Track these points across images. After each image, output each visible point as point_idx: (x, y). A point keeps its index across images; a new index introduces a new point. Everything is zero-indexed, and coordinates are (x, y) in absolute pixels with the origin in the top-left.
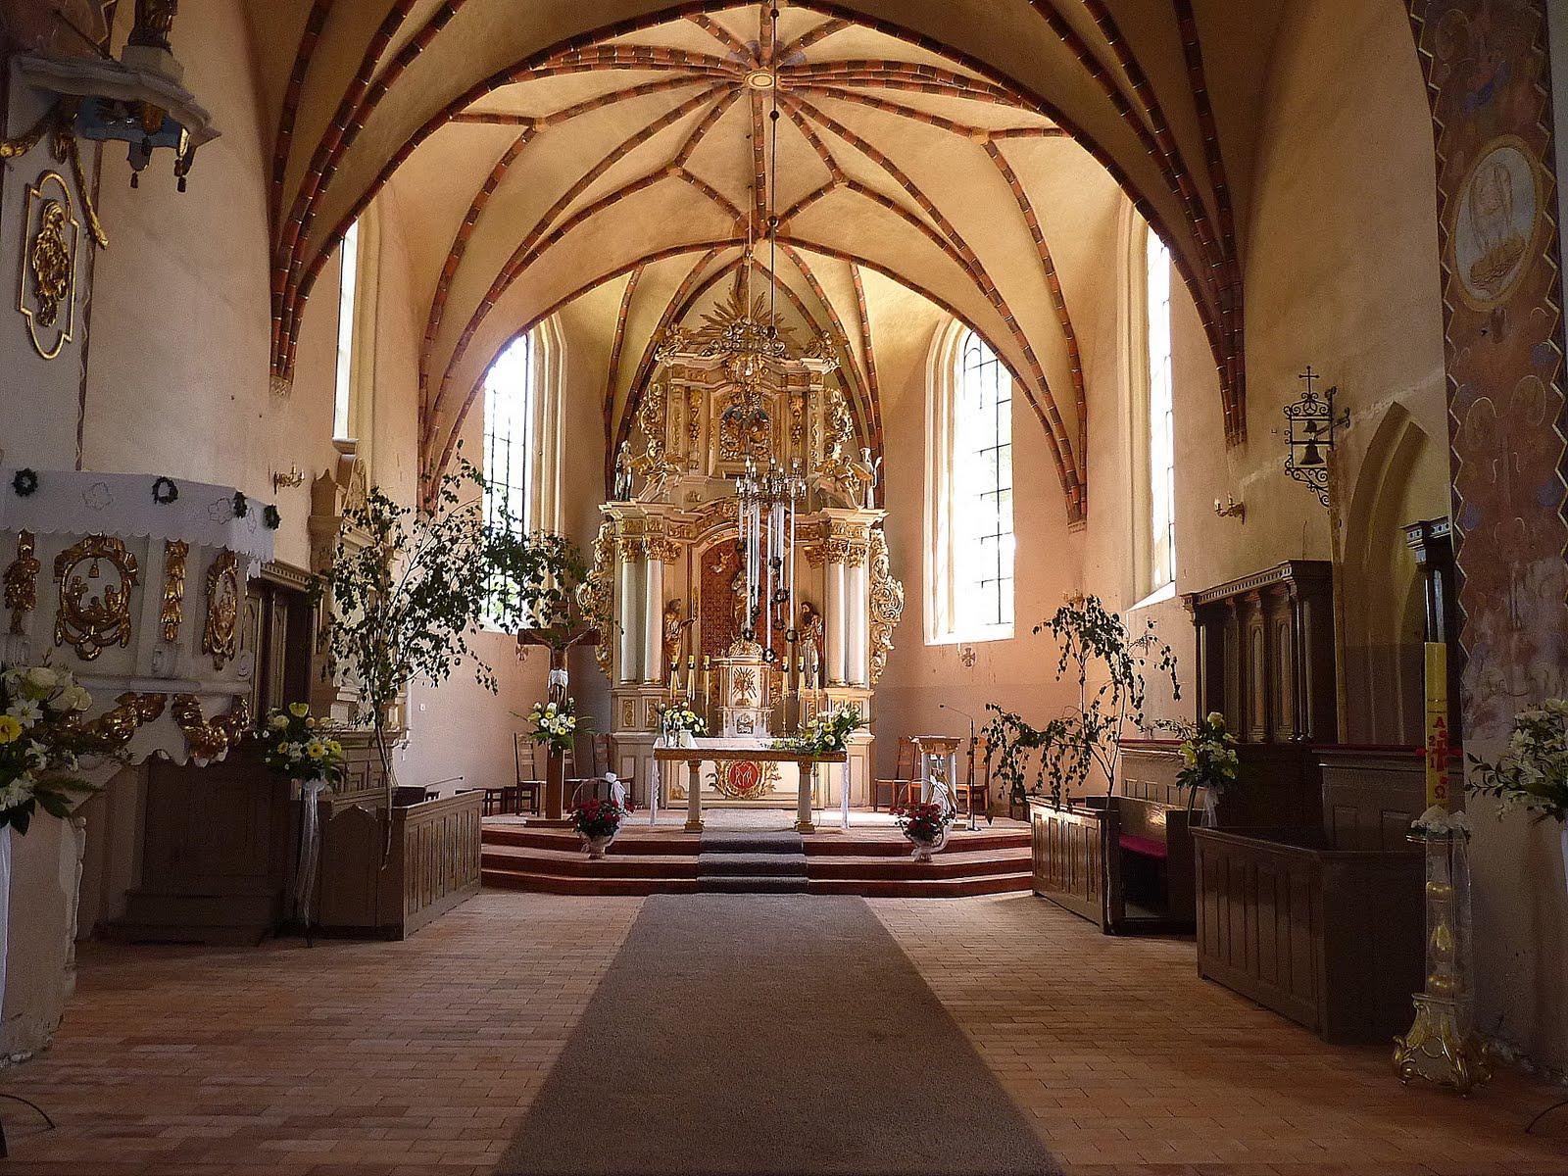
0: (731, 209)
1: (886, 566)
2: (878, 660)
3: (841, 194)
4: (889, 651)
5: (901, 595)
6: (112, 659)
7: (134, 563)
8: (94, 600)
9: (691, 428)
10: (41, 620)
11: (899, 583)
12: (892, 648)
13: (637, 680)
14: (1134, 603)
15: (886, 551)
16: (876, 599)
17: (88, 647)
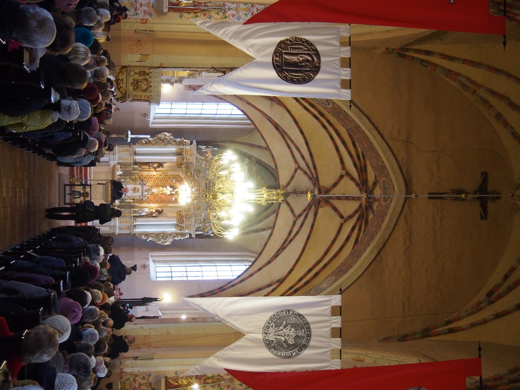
0: (288, 184)
1: (176, 239)
2: (144, 236)
3: (338, 221)
4: (146, 240)
5: (166, 244)
6: (131, 88)
7: (147, 91)
8: (141, 85)
9: (150, 209)
10: (137, 77)
11: (170, 243)
12: (148, 241)
13: (135, 154)
14: (160, 311)
15: (182, 238)
16: (165, 235)
17: (133, 84)
